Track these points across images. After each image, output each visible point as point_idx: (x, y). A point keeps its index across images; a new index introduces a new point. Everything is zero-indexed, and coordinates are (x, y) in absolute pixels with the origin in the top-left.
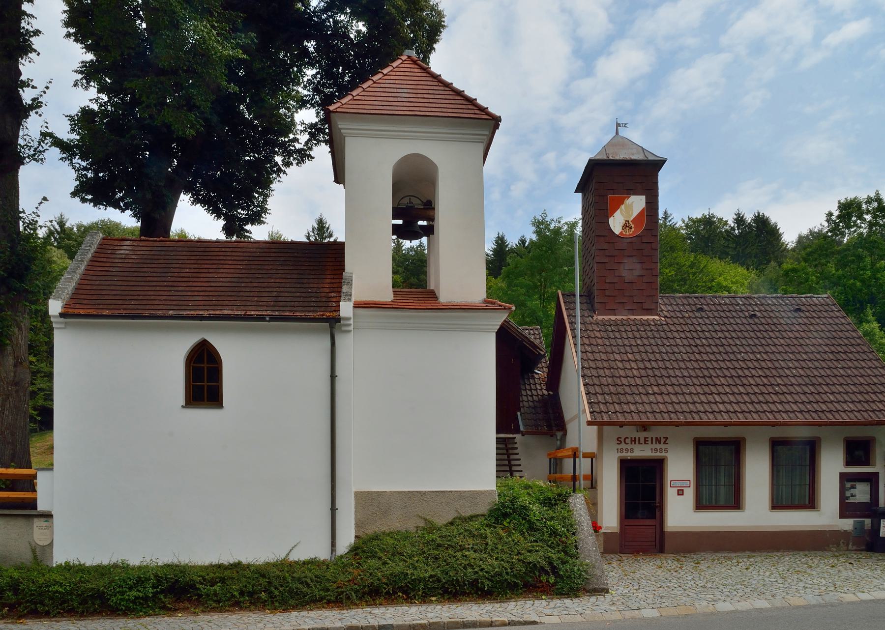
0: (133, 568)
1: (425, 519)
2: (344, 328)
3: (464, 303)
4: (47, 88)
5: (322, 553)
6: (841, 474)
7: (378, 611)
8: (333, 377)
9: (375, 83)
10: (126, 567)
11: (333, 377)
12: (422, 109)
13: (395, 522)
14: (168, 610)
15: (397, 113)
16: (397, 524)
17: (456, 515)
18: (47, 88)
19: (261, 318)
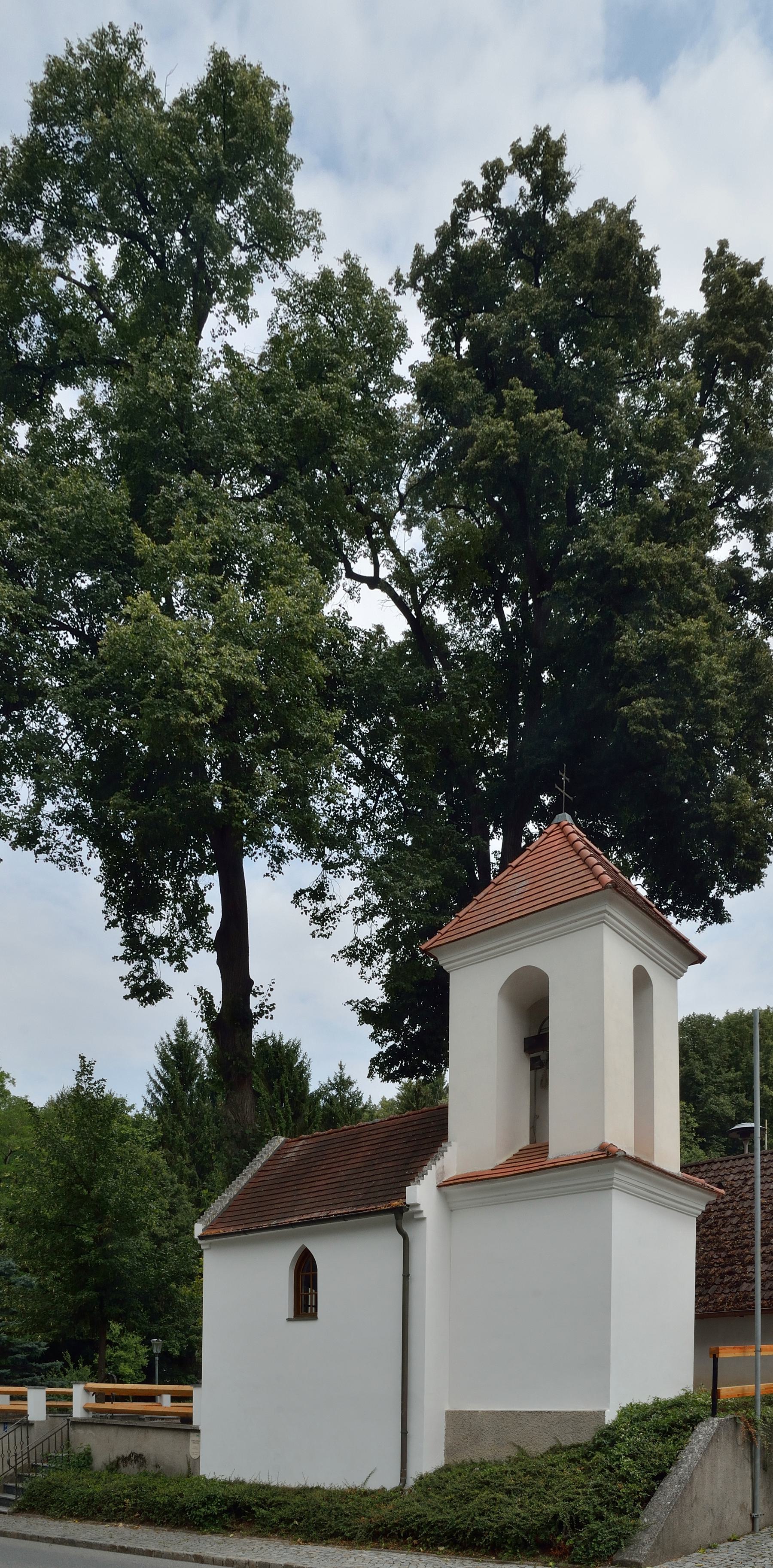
0: (206, 1481)
1: (519, 1447)
2: (416, 1217)
3: (575, 1156)
4: (272, 989)
5: (391, 1481)
6: (447, 1412)
7: (257, 1543)
8: (406, 1276)
9: (497, 885)
10: (243, 1483)
11: (406, 1276)
12: (569, 891)
13: (491, 1451)
14: (227, 1530)
15: (576, 894)
16: (489, 1453)
17: (554, 1443)
18: (272, 989)
19: (328, 1219)
